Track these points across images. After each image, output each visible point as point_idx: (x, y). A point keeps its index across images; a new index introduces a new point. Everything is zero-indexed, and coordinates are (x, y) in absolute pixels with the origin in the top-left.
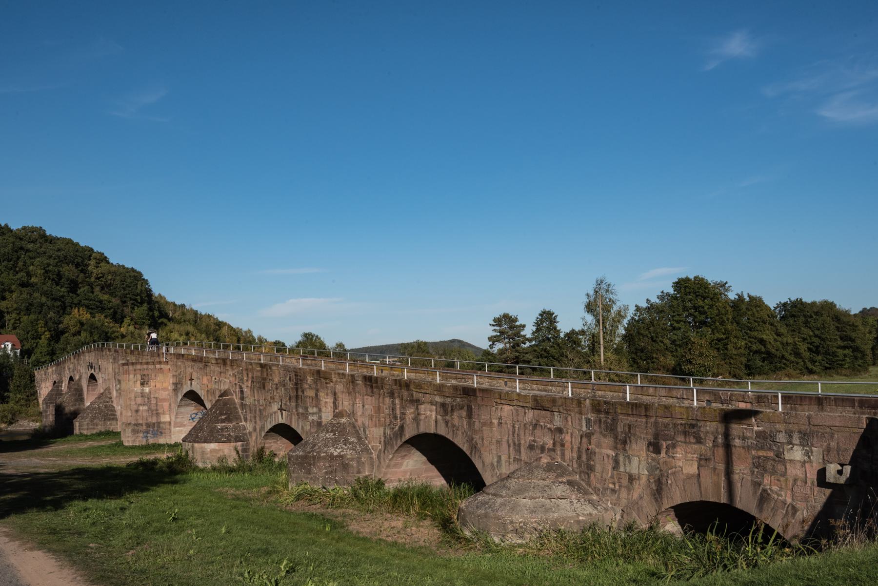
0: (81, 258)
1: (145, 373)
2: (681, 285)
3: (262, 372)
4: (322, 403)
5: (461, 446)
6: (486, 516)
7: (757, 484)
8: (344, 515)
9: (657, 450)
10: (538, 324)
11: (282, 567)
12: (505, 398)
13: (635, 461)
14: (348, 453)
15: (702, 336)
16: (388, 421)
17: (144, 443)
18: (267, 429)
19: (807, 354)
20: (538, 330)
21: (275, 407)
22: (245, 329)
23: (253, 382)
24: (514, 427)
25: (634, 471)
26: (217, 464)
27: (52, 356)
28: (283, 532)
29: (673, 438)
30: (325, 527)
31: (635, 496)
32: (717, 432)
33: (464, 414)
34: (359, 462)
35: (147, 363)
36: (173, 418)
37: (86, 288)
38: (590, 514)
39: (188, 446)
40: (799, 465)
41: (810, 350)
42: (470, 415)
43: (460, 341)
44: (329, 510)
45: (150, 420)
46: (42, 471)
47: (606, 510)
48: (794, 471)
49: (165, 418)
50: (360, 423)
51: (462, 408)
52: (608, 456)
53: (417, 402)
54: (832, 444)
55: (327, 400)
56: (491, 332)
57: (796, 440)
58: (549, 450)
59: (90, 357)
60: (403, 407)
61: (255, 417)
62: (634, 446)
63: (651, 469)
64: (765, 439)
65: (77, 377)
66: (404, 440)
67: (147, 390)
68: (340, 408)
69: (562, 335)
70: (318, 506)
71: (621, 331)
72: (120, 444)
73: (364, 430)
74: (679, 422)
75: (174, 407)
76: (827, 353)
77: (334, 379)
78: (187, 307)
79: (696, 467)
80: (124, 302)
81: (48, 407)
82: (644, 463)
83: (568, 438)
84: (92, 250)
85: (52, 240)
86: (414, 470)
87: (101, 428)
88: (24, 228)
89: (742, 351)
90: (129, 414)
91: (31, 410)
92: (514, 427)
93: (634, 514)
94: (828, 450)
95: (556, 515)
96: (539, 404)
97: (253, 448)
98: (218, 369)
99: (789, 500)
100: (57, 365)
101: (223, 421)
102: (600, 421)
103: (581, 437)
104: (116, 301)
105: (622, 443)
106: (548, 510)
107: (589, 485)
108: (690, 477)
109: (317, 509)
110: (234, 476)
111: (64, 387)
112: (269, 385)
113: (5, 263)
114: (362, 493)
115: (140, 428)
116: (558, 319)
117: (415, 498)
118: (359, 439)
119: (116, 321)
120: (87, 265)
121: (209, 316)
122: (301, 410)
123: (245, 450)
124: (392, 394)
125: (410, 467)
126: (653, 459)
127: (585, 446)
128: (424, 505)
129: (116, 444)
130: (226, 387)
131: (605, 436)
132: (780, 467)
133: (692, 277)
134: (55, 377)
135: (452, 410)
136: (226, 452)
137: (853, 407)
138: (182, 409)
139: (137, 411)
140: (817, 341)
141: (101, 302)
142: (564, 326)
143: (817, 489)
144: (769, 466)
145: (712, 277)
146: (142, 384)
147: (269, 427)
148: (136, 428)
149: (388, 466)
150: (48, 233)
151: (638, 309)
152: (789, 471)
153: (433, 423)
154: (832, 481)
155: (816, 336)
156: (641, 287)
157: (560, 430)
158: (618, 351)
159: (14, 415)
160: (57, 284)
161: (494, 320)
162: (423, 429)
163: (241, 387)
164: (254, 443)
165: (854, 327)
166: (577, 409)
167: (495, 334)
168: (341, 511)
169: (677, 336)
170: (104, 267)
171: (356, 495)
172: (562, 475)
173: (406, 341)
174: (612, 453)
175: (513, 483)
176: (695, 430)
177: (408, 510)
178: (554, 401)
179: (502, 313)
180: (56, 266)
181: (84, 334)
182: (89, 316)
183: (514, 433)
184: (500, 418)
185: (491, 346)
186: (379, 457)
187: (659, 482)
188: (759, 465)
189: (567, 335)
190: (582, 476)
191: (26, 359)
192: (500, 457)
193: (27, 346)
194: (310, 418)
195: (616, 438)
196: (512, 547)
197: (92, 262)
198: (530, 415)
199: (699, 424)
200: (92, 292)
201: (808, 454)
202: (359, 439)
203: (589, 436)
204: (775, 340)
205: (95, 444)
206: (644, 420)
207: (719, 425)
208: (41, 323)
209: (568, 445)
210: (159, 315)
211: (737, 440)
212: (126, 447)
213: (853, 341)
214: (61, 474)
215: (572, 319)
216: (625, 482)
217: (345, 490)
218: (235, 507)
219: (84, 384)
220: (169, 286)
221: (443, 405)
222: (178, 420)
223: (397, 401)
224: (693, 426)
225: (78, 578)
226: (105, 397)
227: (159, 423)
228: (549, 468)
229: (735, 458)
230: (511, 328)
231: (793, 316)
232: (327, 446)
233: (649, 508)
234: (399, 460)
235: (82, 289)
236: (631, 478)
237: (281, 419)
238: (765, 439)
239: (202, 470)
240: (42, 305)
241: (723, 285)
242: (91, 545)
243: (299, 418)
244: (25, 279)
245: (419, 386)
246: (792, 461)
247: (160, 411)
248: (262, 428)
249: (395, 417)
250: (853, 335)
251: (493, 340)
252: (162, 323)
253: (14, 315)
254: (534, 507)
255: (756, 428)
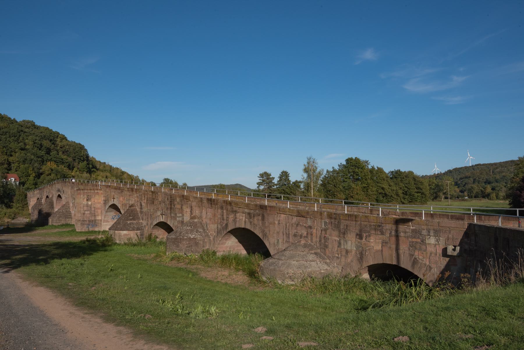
0: (53, 137)
1: (89, 194)
2: (349, 161)
3: (152, 195)
4: (185, 212)
5: (258, 235)
6: (274, 270)
7: (411, 255)
8: (197, 269)
9: (361, 238)
10: (281, 177)
11: (177, 297)
12: (282, 211)
13: (349, 243)
14: (199, 237)
15: (357, 185)
16: (219, 221)
17: (87, 230)
18: (154, 224)
19: (401, 195)
20: (280, 180)
21: (159, 213)
22: (135, 175)
23: (147, 200)
24: (286, 225)
25: (349, 248)
26: (127, 241)
27: (36, 185)
28: (169, 278)
29: (369, 232)
30: (188, 274)
31: (349, 260)
32: (392, 229)
33: (260, 218)
34: (204, 242)
35: (91, 190)
36: (103, 218)
37: (55, 152)
38: (327, 269)
39: (112, 232)
40: (433, 246)
41: (403, 193)
42: (263, 219)
43: (240, 185)
44: (189, 266)
45: (91, 219)
46: (34, 244)
47: (334, 267)
48: (430, 249)
49: (99, 218)
50: (204, 222)
51: (259, 215)
52: (335, 240)
53: (235, 212)
54: (450, 236)
55: (187, 210)
56: (258, 180)
57: (432, 233)
58: (305, 237)
59: (58, 186)
60: (227, 214)
61: (148, 218)
62: (349, 235)
63: (357, 247)
64: (416, 233)
65: (51, 196)
66: (227, 231)
67: (90, 203)
68: (194, 214)
69: (291, 183)
70: (182, 264)
71: (320, 182)
72: (74, 231)
73: (207, 226)
74: (372, 224)
75: (104, 212)
76: (410, 195)
77: (191, 200)
78: (107, 164)
79: (380, 246)
80: (75, 160)
81: (34, 210)
82: (354, 244)
83: (314, 231)
84: (59, 133)
85: (38, 128)
86: (232, 246)
87: (63, 222)
88: (24, 121)
89: (375, 193)
90: (80, 215)
91: (25, 212)
92: (286, 225)
93: (348, 270)
94: (448, 239)
95: (310, 270)
96: (300, 214)
97: (146, 234)
98: (128, 193)
99: (428, 263)
100: (40, 189)
101: (131, 220)
102: (332, 223)
103: (322, 231)
104: (70, 159)
105: (343, 234)
106: (306, 267)
107: (325, 254)
108: (377, 251)
109: (182, 265)
110: (136, 248)
111: (43, 201)
112: (156, 202)
113: (13, 138)
114: (205, 257)
115: (86, 223)
116: (290, 175)
117: (233, 261)
118: (204, 230)
119: (70, 169)
120: (56, 141)
121: (118, 169)
122: (173, 215)
123: (142, 235)
124: (222, 208)
125: (229, 245)
126: (359, 242)
127: (323, 235)
128: (238, 264)
129: (72, 230)
130: (133, 203)
131: (334, 230)
132: (423, 247)
133: (354, 158)
134: (38, 196)
135: (254, 216)
136: (132, 235)
137: (448, 218)
138: (108, 213)
139: (84, 214)
140: (406, 189)
141: (62, 159)
142: (293, 179)
143: (442, 258)
144: (418, 247)
145: (362, 158)
146: (87, 200)
147: (155, 223)
148: (83, 223)
149: (219, 244)
150: (36, 124)
151: (328, 171)
152: (428, 249)
153: (243, 223)
154: (450, 254)
155: (406, 187)
156: (329, 161)
157: (310, 227)
158: (319, 191)
159: (15, 214)
160: (40, 150)
161: (260, 175)
162: (238, 226)
163: (141, 203)
164: (147, 231)
165: (422, 183)
166: (319, 217)
167: (260, 181)
168: (195, 266)
169: (345, 185)
170: (64, 143)
171: (202, 258)
172: (311, 249)
173: (214, 184)
174: (338, 239)
175: (287, 253)
176: (380, 228)
177: (230, 267)
178: (308, 213)
179: (264, 172)
180: (40, 140)
181: (53, 175)
182: (56, 166)
183: (286, 228)
184: (279, 221)
185: (258, 187)
186: (214, 239)
187: (361, 254)
188: (413, 246)
189: (293, 183)
190: (322, 249)
191: (22, 187)
192: (278, 240)
193: (23, 180)
194: (178, 219)
195: (340, 231)
196: (288, 286)
197: (59, 140)
198: (295, 219)
199: (383, 225)
200: (58, 154)
201: (437, 241)
202: (204, 230)
203: (326, 230)
204: (389, 188)
205: (60, 230)
206: (354, 223)
207: (393, 226)
208: (31, 169)
209: (314, 234)
210: (92, 167)
211: (402, 233)
212: (78, 232)
213: (421, 189)
214: (44, 245)
215: (297, 175)
216: (344, 253)
217: (196, 256)
218: (140, 264)
219: (55, 200)
220: (96, 153)
221: (249, 214)
222: (106, 219)
223: (225, 211)
224: (379, 226)
225: (68, 303)
226: (66, 206)
227: (95, 220)
228: (305, 246)
229: (400, 242)
230: (268, 179)
231: (396, 178)
232: (187, 233)
233: (356, 266)
234: (224, 241)
235: (53, 153)
236: (347, 252)
237: (162, 219)
238: (416, 233)
239: (119, 245)
240: (32, 160)
241: (367, 162)
242: (70, 284)
243: (171, 219)
244: (23, 146)
245: (237, 204)
246: (429, 244)
247: (96, 214)
248: (151, 224)
249: (223, 219)
250: (421, 187)
251: (259, 184)
252: (93, 171)
253: (16, 164)
254: (301, 264)
255: (411, 228)
